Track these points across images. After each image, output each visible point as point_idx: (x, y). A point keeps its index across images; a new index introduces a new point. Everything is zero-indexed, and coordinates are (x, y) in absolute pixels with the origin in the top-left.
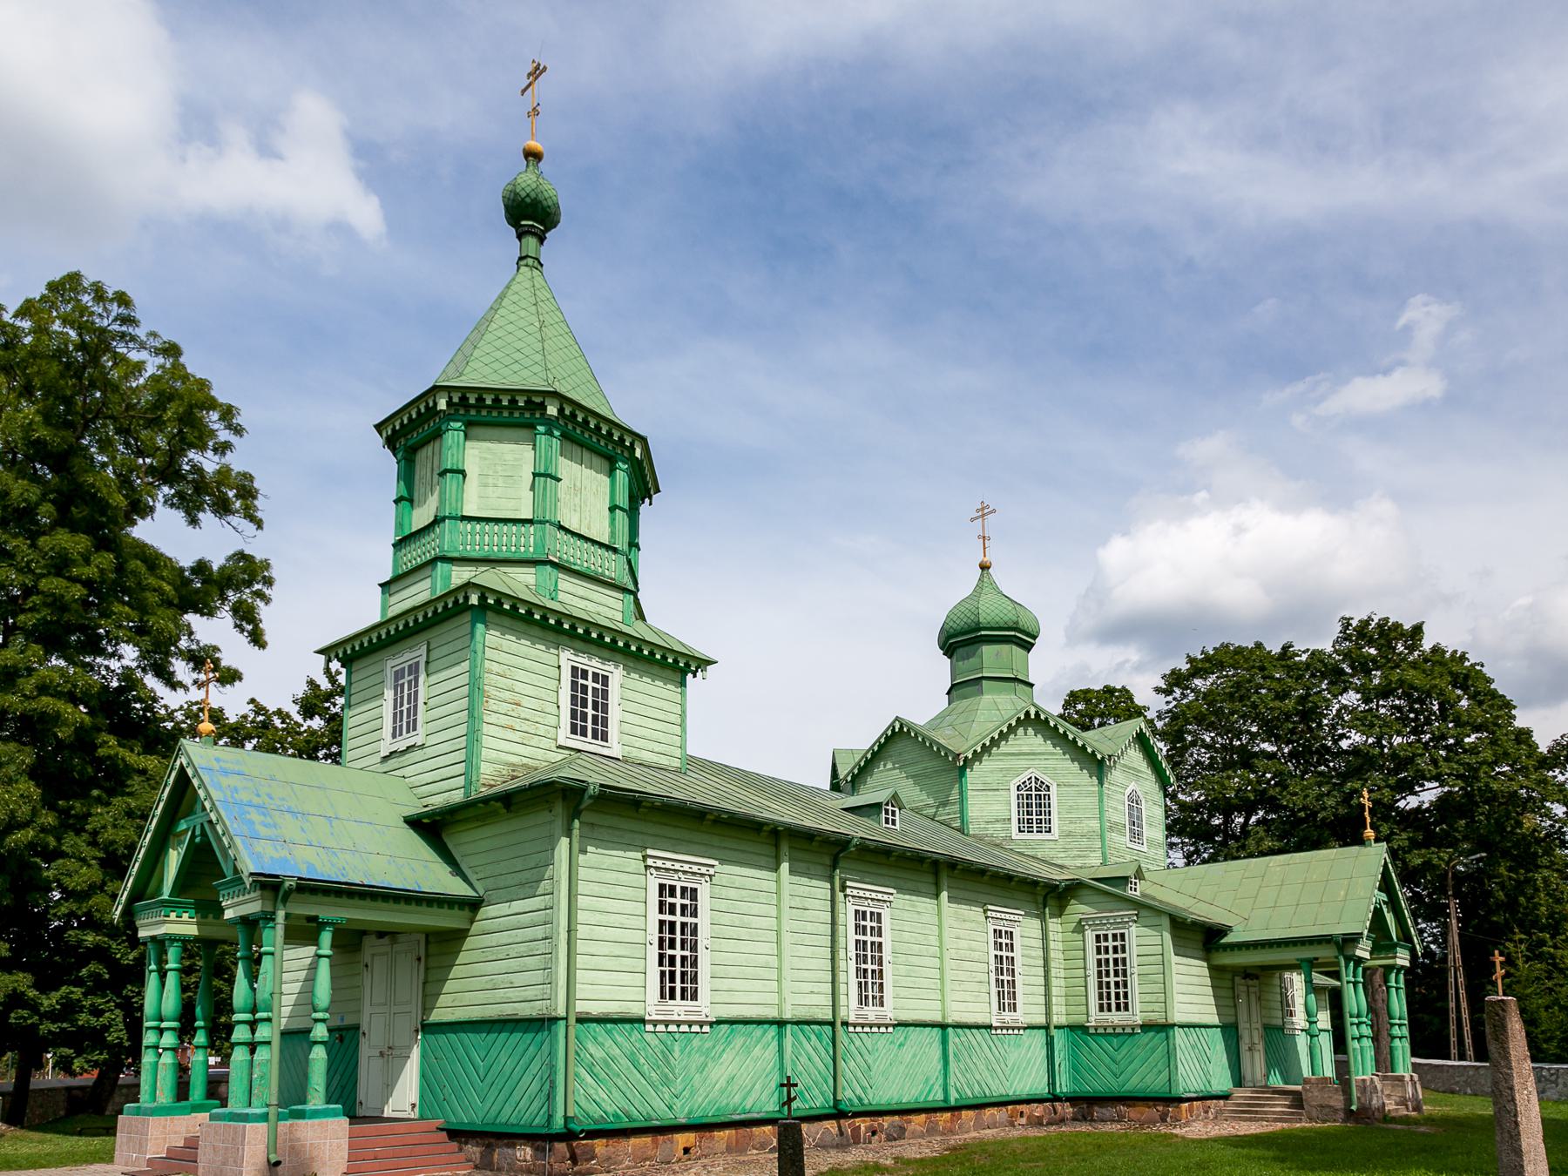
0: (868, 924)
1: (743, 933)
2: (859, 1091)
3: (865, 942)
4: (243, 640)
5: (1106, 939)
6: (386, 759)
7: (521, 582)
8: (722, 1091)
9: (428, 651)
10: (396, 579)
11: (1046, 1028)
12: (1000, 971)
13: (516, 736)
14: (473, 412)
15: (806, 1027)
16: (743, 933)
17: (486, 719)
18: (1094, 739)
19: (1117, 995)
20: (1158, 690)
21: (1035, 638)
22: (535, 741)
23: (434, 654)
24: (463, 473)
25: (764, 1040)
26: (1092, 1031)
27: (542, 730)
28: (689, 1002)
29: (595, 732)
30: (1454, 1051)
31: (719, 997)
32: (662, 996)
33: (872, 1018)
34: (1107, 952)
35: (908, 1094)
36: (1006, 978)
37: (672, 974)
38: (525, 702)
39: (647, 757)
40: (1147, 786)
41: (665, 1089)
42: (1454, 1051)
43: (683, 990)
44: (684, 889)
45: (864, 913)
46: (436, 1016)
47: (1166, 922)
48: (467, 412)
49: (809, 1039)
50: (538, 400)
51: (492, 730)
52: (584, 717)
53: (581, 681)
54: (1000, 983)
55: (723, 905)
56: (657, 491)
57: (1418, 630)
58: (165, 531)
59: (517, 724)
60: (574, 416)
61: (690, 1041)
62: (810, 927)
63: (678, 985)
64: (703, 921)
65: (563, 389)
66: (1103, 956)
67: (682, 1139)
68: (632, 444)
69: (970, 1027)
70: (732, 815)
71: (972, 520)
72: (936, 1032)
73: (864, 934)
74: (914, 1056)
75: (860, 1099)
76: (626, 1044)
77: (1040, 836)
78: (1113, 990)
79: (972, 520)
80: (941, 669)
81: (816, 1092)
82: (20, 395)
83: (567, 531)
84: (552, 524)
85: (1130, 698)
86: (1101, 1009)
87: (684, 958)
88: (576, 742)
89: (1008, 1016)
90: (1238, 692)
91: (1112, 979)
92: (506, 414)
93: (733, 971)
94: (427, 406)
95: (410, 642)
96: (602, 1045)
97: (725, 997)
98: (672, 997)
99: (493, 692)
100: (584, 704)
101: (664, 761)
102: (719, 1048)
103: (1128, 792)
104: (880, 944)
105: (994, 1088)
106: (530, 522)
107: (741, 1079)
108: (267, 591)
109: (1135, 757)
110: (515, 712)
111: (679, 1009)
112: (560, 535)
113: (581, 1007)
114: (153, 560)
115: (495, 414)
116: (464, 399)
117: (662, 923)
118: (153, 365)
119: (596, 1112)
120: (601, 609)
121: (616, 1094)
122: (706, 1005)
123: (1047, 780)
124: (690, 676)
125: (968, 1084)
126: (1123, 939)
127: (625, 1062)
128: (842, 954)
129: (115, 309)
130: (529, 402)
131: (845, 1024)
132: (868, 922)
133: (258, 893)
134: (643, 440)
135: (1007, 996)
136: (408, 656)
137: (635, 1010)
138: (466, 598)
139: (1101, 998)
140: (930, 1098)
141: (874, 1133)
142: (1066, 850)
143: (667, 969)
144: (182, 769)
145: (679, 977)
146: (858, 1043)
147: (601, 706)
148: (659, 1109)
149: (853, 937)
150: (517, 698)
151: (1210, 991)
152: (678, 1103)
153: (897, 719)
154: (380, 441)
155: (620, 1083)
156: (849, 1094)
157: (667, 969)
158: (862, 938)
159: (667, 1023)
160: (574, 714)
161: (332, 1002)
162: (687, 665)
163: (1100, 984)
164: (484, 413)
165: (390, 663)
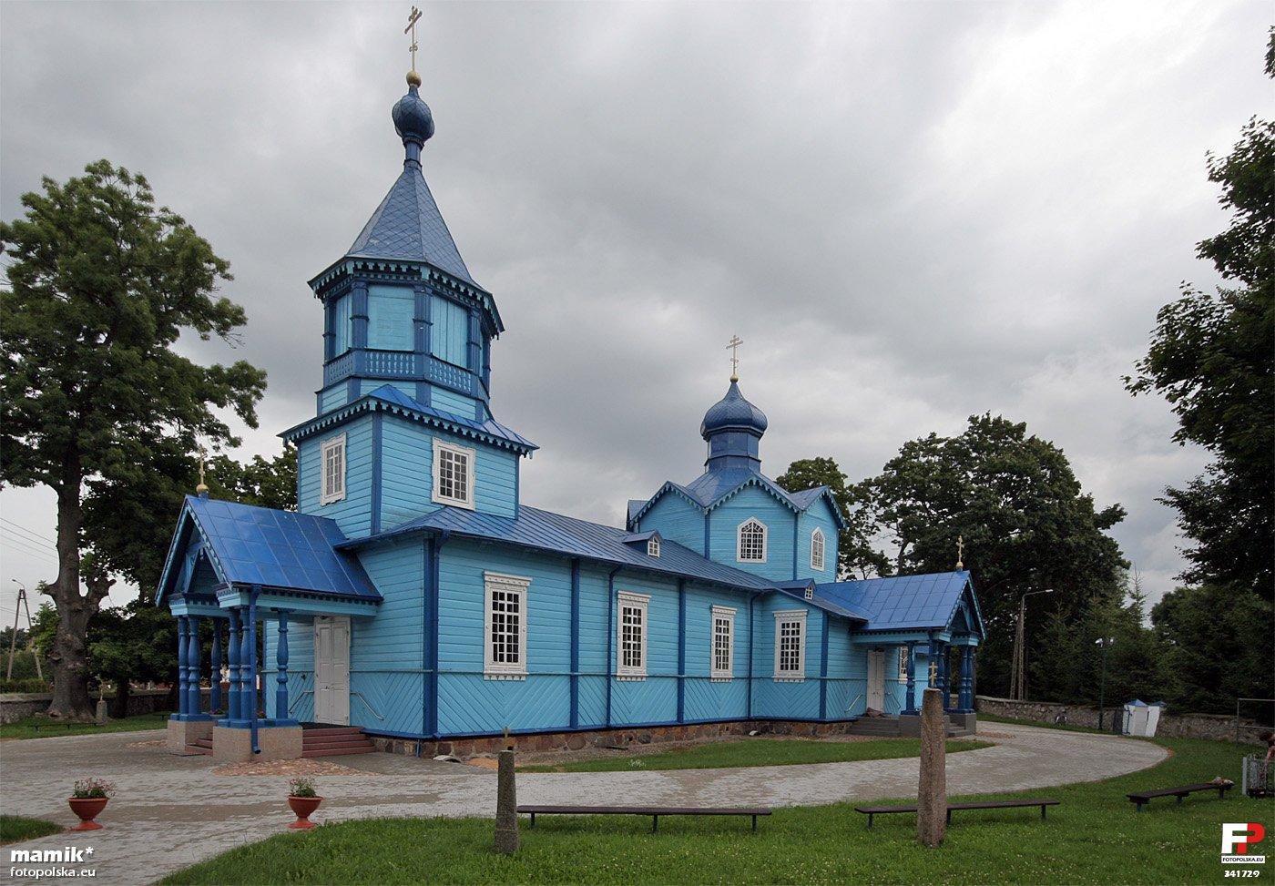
3: (629, 628)
4: (241, 420)
5: (502, 598)
9: (347, 439)
10: (325, 390)
12: (718, 645)
14: (372, 276)
15: (453, 678)
18: (796, 499)
19: (792, 660)
24: (367, 319)
26: (776, 681)
29: (457, 493)
30: (1012, 693)
34: (788, 634)
36: (722, 649)
37: (502, 646)
42: (1012, 693)
43: (509, 656)
44: (509, 595)
46: (703, 553)
48: (368, 275)
50: (415, 268)
52: (450, 484)
56: (503, 330)
57: (1022, 427)
58: (189, 346)
60: (440, 279)
63: (505, 653)
64: (522, 614)
65: (433, 260)
66: (785, 637)
68: (482, 299)
73: (629, 622)
77: (754, 561)
78: (790, 657)
80: (703, 450)
85: (835, 467)
86: (782, 668)
87: (509, 637)
91: (790, 651)
94: (341, 271)
95: (336, 432)
98: (502, 660)
100: (450, 475)
103: (814, 533)
109: (819, 511)
110: (414, 479)
114: (184, 368)
116: (365, 266)
117: (495, 616)
118: (167, 231)
124: (522, 456)
126: (798, 627)
130: (409, 269)
133: (239, 594)
134: (490, 296)
136: (334, 441)
141: (631, 739)
143: (498, 643)
144: (189, 516)
149: (621, 624)
154: (312, 292)
157: (498, 643)
158: (719, 634)
160: (443, 481)
162: (519, 450)
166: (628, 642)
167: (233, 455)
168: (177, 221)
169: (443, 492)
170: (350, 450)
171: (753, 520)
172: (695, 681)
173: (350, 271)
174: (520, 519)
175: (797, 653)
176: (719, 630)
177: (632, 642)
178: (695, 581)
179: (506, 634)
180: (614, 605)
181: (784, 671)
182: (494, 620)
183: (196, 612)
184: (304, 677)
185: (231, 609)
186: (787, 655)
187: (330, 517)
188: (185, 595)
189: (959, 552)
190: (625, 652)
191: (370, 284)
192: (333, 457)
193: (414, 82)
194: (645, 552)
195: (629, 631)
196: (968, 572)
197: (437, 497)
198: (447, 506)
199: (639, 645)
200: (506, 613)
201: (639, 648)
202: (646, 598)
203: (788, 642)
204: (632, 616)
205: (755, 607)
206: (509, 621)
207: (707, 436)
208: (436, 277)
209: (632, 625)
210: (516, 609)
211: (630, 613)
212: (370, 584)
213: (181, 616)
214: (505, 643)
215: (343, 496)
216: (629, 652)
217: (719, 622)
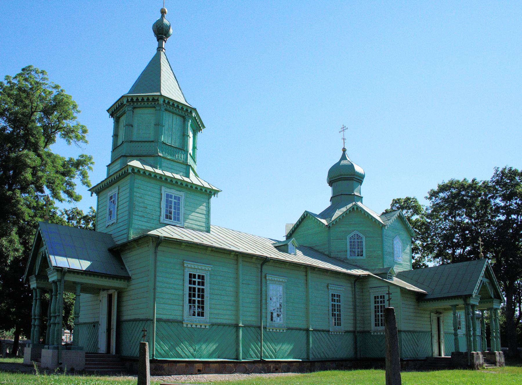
0: (336, 298)
3: (194, 288)
5: (195, 277)
9: (119, 189)
11: (354, 332)
14: (135, 104)
17: (134, 213)
20: (426, 198)
23: (120, 191)
24: (132, 126)
36: (336, 313)
45: (335, 295)
47: (399, 290)
51: (136, 217)
52: (171, 213)
53: (170, 199)
54: (333, 315)
64: (207, 287)
66: (377, 305)
69: (319, 331)
70: (217, 248)
71: (340, 132)
73: (335, 302)
79: (340, 132)
82: (15, 105)
86: (376, 325)
87: (198, 301)
99: (136, 203)
100: (171, 208)
106: (152, 141)
117: (190, 288)
118: (55, 92)
123: (361, 235)
125: (319, 353)
129: (41, 75)
134: (195, 109)
139: (376, 321)
153: (306, 211)
154: (108, 114)
158: (333, 303)
162: (210, 192)
163: (376, 315)
169: (167, 217)
171: (356, 232)
173: (125, 102)
176: (333, 300)
178: (317, 269)
179: (196, 299)
180: (264, 284)
182: (375, 308)
183: (40, 286)
184: (94, 326)
186: (378, 317)
188: (36, 276)
191: (134, 108)
193: (163, 12)
199: (340, 314)
200: (197, 286)
201: (340, 316)
202: (208, 268)
203: (378, 308)
204: (336, 298)
205: (357, 286)
206: (199, 291)
207: (331, 182)
209: (336, 303)
210: (203, 284)
211: (199, 282)
212: (126, 270)
213: (34, 288)
215: (115, 221)
217: (333, 295)
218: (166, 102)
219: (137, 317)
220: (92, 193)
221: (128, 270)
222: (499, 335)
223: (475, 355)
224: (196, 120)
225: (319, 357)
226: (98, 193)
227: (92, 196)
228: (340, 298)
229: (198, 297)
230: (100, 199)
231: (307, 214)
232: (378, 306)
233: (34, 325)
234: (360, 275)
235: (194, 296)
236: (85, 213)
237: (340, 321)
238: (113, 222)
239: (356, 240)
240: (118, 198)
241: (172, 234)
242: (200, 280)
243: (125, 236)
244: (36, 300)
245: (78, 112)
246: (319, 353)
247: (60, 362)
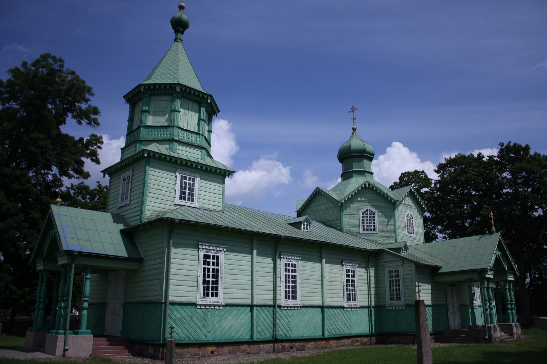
0: (350, 274)
1: (238, 272)
2: (285, 332)
3: (209, 269)
6: (119, 208)
7: (163, 149)
8: (227, 331)
9: (133, 172)
13: (159, 201)
14: (163, 91)
16: (238, 272)
19: (397, 294)
21: (373, 155)
22: (166, 202)
23: (135, 173)
25: (245, 312)
27: (169, 198)
28: (215, 298)
31: (226, 296)
32: (204, 295)
33: (291, 304)
35: (307, 334)
36: (351, 288)
37: (208, 287)
38: (163, 189)
39: (209, 207)
40: (414, 211)
41: (204, 329)
45: (349, 270)
47: (413, 265)
49: (264, 312)
50: (173, 86)
51: (151, 199)
52: (185, 193)
53: (184, 181)
54: (348, 290)
55: (229, 262)
56: (219, 111)
59: (160, 197)
61: (215, 312)
62: (265, 270)
63: (210, 291)
66: (391, 279)
67: (210, 349)
68: (207, 98)
72: (320, 310)
73: (349, 277)
74: (310, 318)
75: (285, 335)
76: (190, 313)
78: (395, 292)
81: (266, 332)
83: (182, 129)
84: (176, 127)
87: (213, 282)
88: (182, 202)
89: (352, 303)
90: (463, 172)
92: (163, 91)
93: (233, 286)
96: (179, 313)
97: (229, 296)
98: (208, 295)
99: (151, 185)
100: (185, 189)
101: (215, 208)
102: (226, 315)
103: (407, 214)
104: (295, 276)
105: (345, 331)
107: (235, 326)
108: (101, 146)
109: (408, 201)
111: (210, 300)
112: (180, 131)
113: (171, 299)
115: (160, 91)
118: (70, 77)
119: (196, 337)
120: (193, 155)
121: (185, 330)
122: (220, 300)
125: (334, 330)
127: (188, 319)
128: (278, 280)
131: (280, 307)
132: (291, 268)
134: (211, 96)
135: (351, 295)
136: (127, 173)
137: (193, 300)
138: (143, 154)
139: (391, 295)
140: (317, 335)
141: (291, 348)
142: (381, 237)
143: (206, 285)
145: (211, 287)
146: (285, 313)
147: (192, 189)
148: (202, 336)
149: (283, 273)
150: (160, 187)
151: (430, 295)
152: (209, 335)
153: (317, 188)
154: (124, 100)
155: (186, 327)
156: (281, 332)
158: (348, 278)
159: (205, 305)
160: (181, 192)
161: (90, 294)
162: (225, 173)
164: (156, 91)
165: (122, 176)
166: (288, 284)
167: (87, 182)
168: (73, 73)
170: (134, 177)
172: (334, 309)
174: (225, 212)
175: (399, 289)
176: (348, 276)
177: (291, 284)
181: (392, 302)
185: (63, 265)
187: (121, 214)
189: (493, 224)
190: (286, 291)
192: (126, 182)
194: (300, 228)
195: (289, 278)
196: (499, 233)
197: (178, 201)
198: (182, 206)
199: (355, 289)
200: (211, 267)
204: (350, 274)
208: (183, 89)
213: (40, 270)
214: (211, 285)
216: (289, 291)
218: (183, 89)
219: (149, 299)
220: (104, 175)
221: (141, 251)
222: (513, 306)
223: (492, 328)
224: (212, 105)
225: (334, 333)
226: (110, 175)
227: (104, 177)
228: (354, 273)
229: (213, 277)
230: (112, 180)
231: (319, 191)
232: (393, 280)
233: (38, 308)
234: (374, 250)
235: (208, 277)
236: (91, 188)
237: (355, 296)
238: (125, 203)
239: (369, 215)
240: (132, 180)
241: (187, 215)
242: (215, 261)
243: (138, 217)
244: (42, 282)
245: (92, 95)
246: (334, 330)
247: (66, 348)
